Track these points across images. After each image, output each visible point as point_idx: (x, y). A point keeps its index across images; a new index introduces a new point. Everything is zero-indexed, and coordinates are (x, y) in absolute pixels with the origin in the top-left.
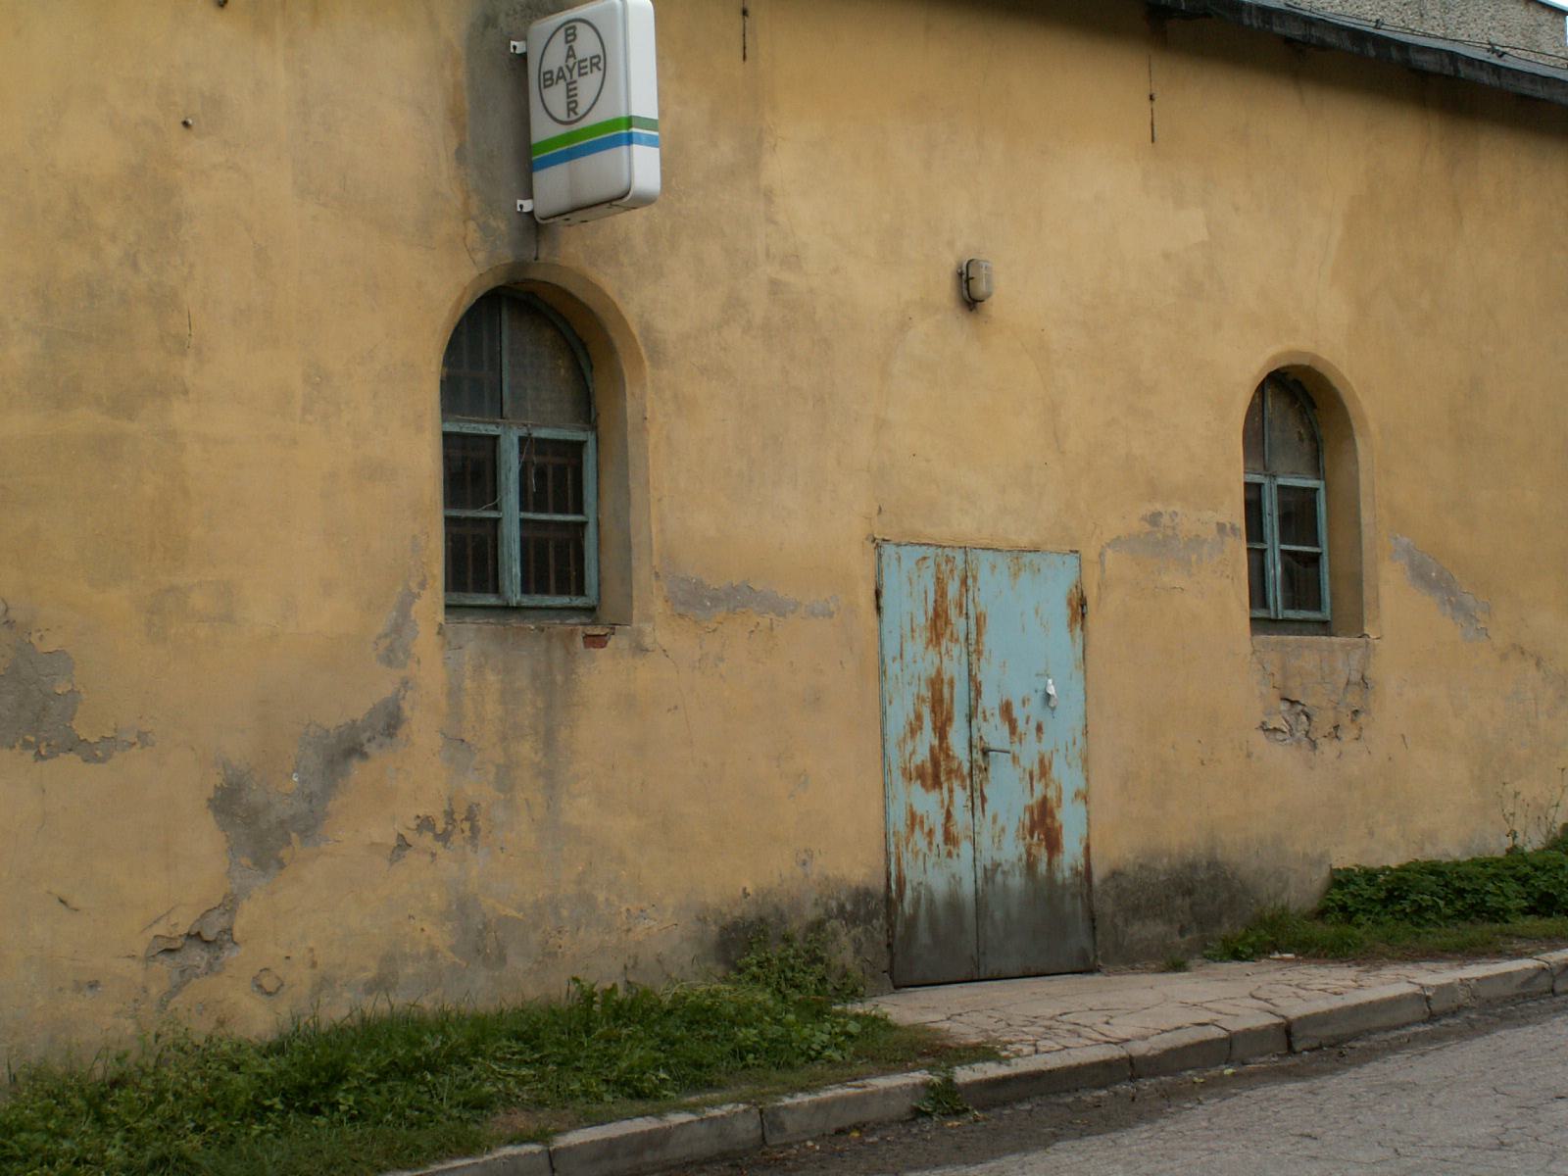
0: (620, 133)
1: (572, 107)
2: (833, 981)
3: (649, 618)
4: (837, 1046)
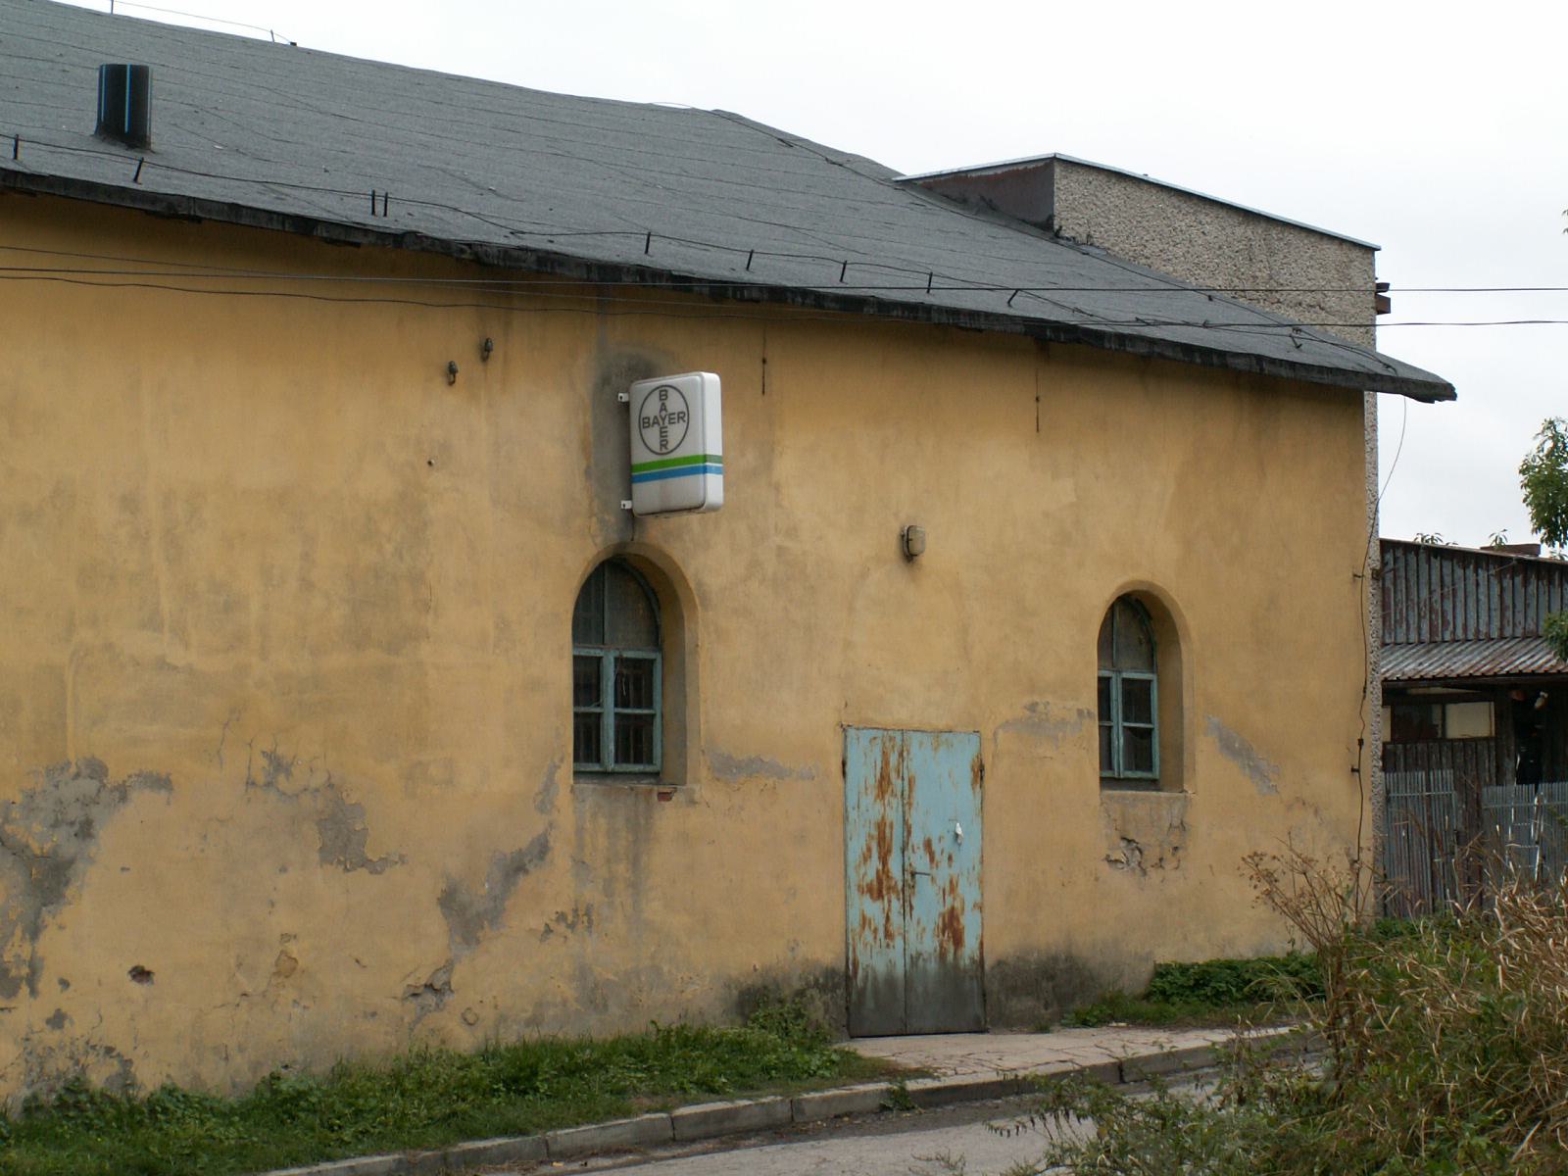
0: (698, 466)
1: (664, 443)
2: (811, 1031)
3: (697, 781)
4: (827, 1068)
